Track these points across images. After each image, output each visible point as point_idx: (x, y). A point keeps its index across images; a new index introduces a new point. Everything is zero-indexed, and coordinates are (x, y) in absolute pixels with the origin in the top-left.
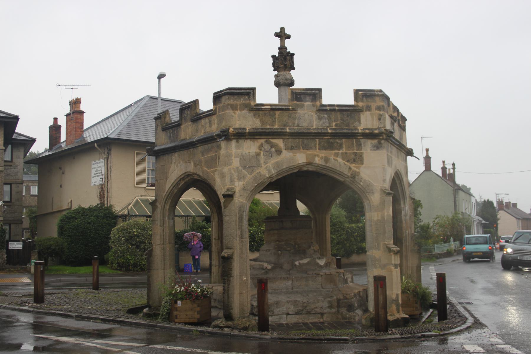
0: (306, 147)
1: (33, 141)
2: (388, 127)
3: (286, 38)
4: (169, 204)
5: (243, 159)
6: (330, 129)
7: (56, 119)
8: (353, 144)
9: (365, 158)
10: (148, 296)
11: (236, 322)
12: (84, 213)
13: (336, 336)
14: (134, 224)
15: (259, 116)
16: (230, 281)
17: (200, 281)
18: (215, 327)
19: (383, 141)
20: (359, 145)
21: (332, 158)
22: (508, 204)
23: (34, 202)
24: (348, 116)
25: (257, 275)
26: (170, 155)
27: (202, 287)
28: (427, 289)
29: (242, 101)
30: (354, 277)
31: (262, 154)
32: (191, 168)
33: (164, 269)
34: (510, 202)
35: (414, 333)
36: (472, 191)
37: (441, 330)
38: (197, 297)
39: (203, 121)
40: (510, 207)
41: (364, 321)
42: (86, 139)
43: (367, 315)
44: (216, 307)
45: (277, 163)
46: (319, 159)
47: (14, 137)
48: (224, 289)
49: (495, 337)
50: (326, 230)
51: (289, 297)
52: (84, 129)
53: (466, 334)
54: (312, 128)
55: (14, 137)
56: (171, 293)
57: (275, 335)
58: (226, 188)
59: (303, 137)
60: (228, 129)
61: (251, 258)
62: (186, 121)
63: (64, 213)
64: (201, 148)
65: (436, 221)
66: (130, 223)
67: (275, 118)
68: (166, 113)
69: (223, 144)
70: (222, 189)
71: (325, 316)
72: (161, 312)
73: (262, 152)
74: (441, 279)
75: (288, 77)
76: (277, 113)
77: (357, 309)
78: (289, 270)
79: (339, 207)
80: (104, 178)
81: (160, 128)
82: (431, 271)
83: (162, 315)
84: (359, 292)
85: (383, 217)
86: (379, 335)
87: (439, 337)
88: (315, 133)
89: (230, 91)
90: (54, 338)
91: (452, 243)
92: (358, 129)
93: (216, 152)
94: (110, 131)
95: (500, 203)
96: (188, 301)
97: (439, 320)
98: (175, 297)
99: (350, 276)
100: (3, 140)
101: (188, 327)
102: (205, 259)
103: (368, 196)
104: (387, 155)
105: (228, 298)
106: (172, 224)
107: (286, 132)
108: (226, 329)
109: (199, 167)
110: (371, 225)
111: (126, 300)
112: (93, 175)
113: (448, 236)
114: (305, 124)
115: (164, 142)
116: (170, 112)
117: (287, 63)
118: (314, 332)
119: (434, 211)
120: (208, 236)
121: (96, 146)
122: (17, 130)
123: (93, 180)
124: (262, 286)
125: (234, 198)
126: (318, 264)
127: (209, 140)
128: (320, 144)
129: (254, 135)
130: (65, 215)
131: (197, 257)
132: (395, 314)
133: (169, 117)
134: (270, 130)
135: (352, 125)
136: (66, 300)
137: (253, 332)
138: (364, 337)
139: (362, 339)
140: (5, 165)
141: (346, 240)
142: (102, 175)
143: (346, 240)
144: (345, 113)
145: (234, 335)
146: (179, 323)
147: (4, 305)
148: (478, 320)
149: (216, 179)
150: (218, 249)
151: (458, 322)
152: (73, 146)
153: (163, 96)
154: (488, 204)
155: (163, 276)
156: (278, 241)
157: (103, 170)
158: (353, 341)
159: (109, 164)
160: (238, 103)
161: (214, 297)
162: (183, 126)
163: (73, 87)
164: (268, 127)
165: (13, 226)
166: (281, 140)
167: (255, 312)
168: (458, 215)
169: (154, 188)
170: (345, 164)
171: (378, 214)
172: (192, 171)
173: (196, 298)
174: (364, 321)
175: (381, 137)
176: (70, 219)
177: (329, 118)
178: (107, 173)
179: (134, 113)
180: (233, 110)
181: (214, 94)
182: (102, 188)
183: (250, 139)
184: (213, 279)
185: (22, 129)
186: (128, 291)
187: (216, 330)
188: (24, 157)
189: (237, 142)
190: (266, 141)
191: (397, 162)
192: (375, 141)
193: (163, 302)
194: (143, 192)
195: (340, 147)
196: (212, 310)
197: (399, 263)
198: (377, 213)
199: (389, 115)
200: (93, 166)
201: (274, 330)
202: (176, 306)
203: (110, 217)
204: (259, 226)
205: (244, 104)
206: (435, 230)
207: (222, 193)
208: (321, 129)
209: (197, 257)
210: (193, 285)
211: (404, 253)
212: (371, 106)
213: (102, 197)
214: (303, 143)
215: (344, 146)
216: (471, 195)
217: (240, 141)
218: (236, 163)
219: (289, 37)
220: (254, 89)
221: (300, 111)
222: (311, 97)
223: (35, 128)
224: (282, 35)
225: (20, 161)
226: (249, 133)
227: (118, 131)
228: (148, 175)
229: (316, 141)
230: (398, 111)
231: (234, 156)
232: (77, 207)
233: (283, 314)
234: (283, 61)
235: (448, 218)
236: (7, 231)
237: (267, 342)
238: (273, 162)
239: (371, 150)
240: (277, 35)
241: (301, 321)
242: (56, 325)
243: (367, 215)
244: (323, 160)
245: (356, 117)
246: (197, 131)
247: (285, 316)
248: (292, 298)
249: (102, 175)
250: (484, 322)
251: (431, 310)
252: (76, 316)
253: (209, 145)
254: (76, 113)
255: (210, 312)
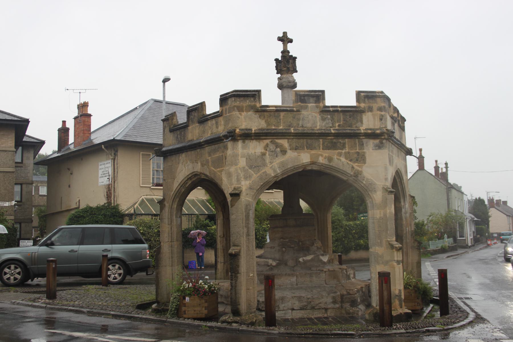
0: (310, 147)
1: (42, 143)
2: (389, 127)
3: (288, 42)
4: (176, 203)
5: (249, 158)
6: (334, 130)
7: (64, 122)
8: (355, 144)
9: (367, 157)
10: (157, 292)
11: (243, 317)
12: (92, 211)
13: (342, 331)
14: (140, 222)
15: (264, 117)
16: (237, 277)
17: (207, 277)
18: (223, 322)
19: (384, 141)
20: (362, 145)
21: (335, 157)
22: (498, 201)
23: (43, 202)
24: (350, 117)
25: (262, 271)
26: (178, 155)
27: (210, 283)
28: (428, 284)
29: (248, 102)
30: (356, 273)
31: (267, 154)
32: (198, 168)
33: (172, 266)
34: (500, 200)
35: (419, 328)
36: (463, 190)
37: (444, 325)
38: (205, 293)
39: (209, 123)
40: (500, 205)
41: (367, 316)
42: (94, 141)
43: (370, 310)
44: (223, 303)
45: (282, 163)
46: (323, 158)
47: (25, 139)
48: (231, 286)
49: (498, 332)
50: (327, 228)
51: (294, 293)
52: (92, 131)
53: (469, 329)
54: (315, 129)
55: (25, 139)
56: (179, 289)
57: (282, 330)
58: (233, 187)
59: (306, 137)
60: (235, 130)
61: (257, 255)
62: (193, 122)
63: (73, 212)
64: (208, 149)
65: (430, 218)
66: (136, 221)
67: (280, 119)
68: (173, 115)
69: (230, 144)
70: (228, 188)
71: (329, 312)
72: (170, 308)
73: (267, 152)
74: (443, 275)
75: (291, 79)
76: (282, 114)
77: (360, 304)
78: (293, 267)
79: (337, 205)
80: (110, 178)
81: (167, 130)
82: (427, 267)
83: (171, 311)
84: (362, 287)
85: (385, 215)
86: (384, 330)
87: (443, 332)
88: (319, 133)
89: (236, 93)
90: (68, 333)
91: (446, 239)
92: (360, 130)
93: (223, 152)
94: (116, 133)
95: (491, 201)
96: (196, 296)
97: (441, 315)
98: (183, 294)
99: (352, 272)
100: (14, 141)
101: (197, 323)
102: (209, 256)
103: (370, 194)
104: (389, 154)
105: (236, 294)
106: (179, 222)
107: (291, 133)
108: (234, 324)
109: (206, 166)
110: (374, 223)
111: (135, 296)
112: (100, 176)
113: (441, 233)
114: (309, 125)
115: (172, 143)
116: (177, 113)
117: (290, 66)
118: (320, 327)
119: (427, 208)
120: (211, 233)
121: (103, 147)
122: (28, 133)
123: (101, 180)
124: (269, 282)
125: (241, 197)
126: (321, 260)
127: (215, 141)
128: (323, 144)
129: (259, 136)
130: (73, 214)
131: (201, 254)
132: (399, 309)
133: (177, 119)
134: (275, 131)
135: (355, 126)
136: (77, 296)
137: (261, 327)
138: (369, 332)
139: (368, 334)
140: (16, 167)
141: (345, 237)
142: (109, 175)
143: (345, 237)
144: (348, 114)
145: (242, 330)
146: (189, 318)
147: (18, 302)
148: (479, 315)
149: (223, 178)
150: (223, 246)
151: (461, 317)
152: (81, 148)
153: (168, 99)
154: (479, 202)
155: (171, 273)
156: (282, 238)
157: (110, 171)
158: (360, 336)
159: (116, 165)
160: (244, 105)
161: (221, 293)
162: (190, 128)
163: (81, 91)
164: (273, 128)
165: (23, 225)
166: (286, 140)
167: (261, 308)
168: (451, 213)
169: (162, 188)
170: (347, 163)
171: (380, 212)
172: (199, 171)
173: (203, 294)
174: (367, 316)
175: (383, 137)
176: (78, 217)
177: (332, 119)
178: (114, 174)
179: (140, 116)
180: (239, 111)
181: (221, 96)
182: (109, 188)
183: (256, 139)
184: (219, 275)
185: (31, 132)
186: (137, 287)
187: (224, 325)
188: (34, 159)
189: (244, 142)
190: (272, 141)
191: (397, 162)
192: (377, 141)
193: (172, 298)
194: (148, 191)
195: (343, 147)
196: (219, 306)
197: (401, 259)
198: (379, 212)
199: (390, 116)
200: (100, 167)
201: (280, 325)
202: (184, 302)
203: (117, 216)
204: (260, 224)
205: (249, 106)
206: (429, 228)
207: (229, 192)
208: (324, 129)
209: (201, 254)
210: (201, 281)
211: (405, 250)
212: (372, 107)
213: (109, 196)
214: (307, 143)
215: (347, 146)
216: (462, 193)
217: (247, 141)
218: (242, 162)
219: (291, 41)
220: (259, 92)
221: (304, 113)
222: (315, 99)
223: (44, 130)
224: (285, 39)
225: (30, 162)
226: (255, 133)
227: (124, 133)
228: (153, 175)
229: (320, 141)
230: (398, 112)
231: (240, 156)
232: (85, 206)
233: (288, 309)
234: (286, 64)
235: (441, 215)
236: (18, 229)
237: (275, 336)
238: (278, 161)
239: (373, 150)
240: (280, 39)
241: (305, 316)
242: (70, 320)
243: (370, 212)
244: (326, 159)
245: (358, 117)
246: (204, 132)
247: (290, 311)
248: (297, 294)
249: (109, 175)
250: (485, 317)
251: (431, 305)
252: (88, 311)
253: (216, 146)
254: (83, 116)
255: (217, 307)
